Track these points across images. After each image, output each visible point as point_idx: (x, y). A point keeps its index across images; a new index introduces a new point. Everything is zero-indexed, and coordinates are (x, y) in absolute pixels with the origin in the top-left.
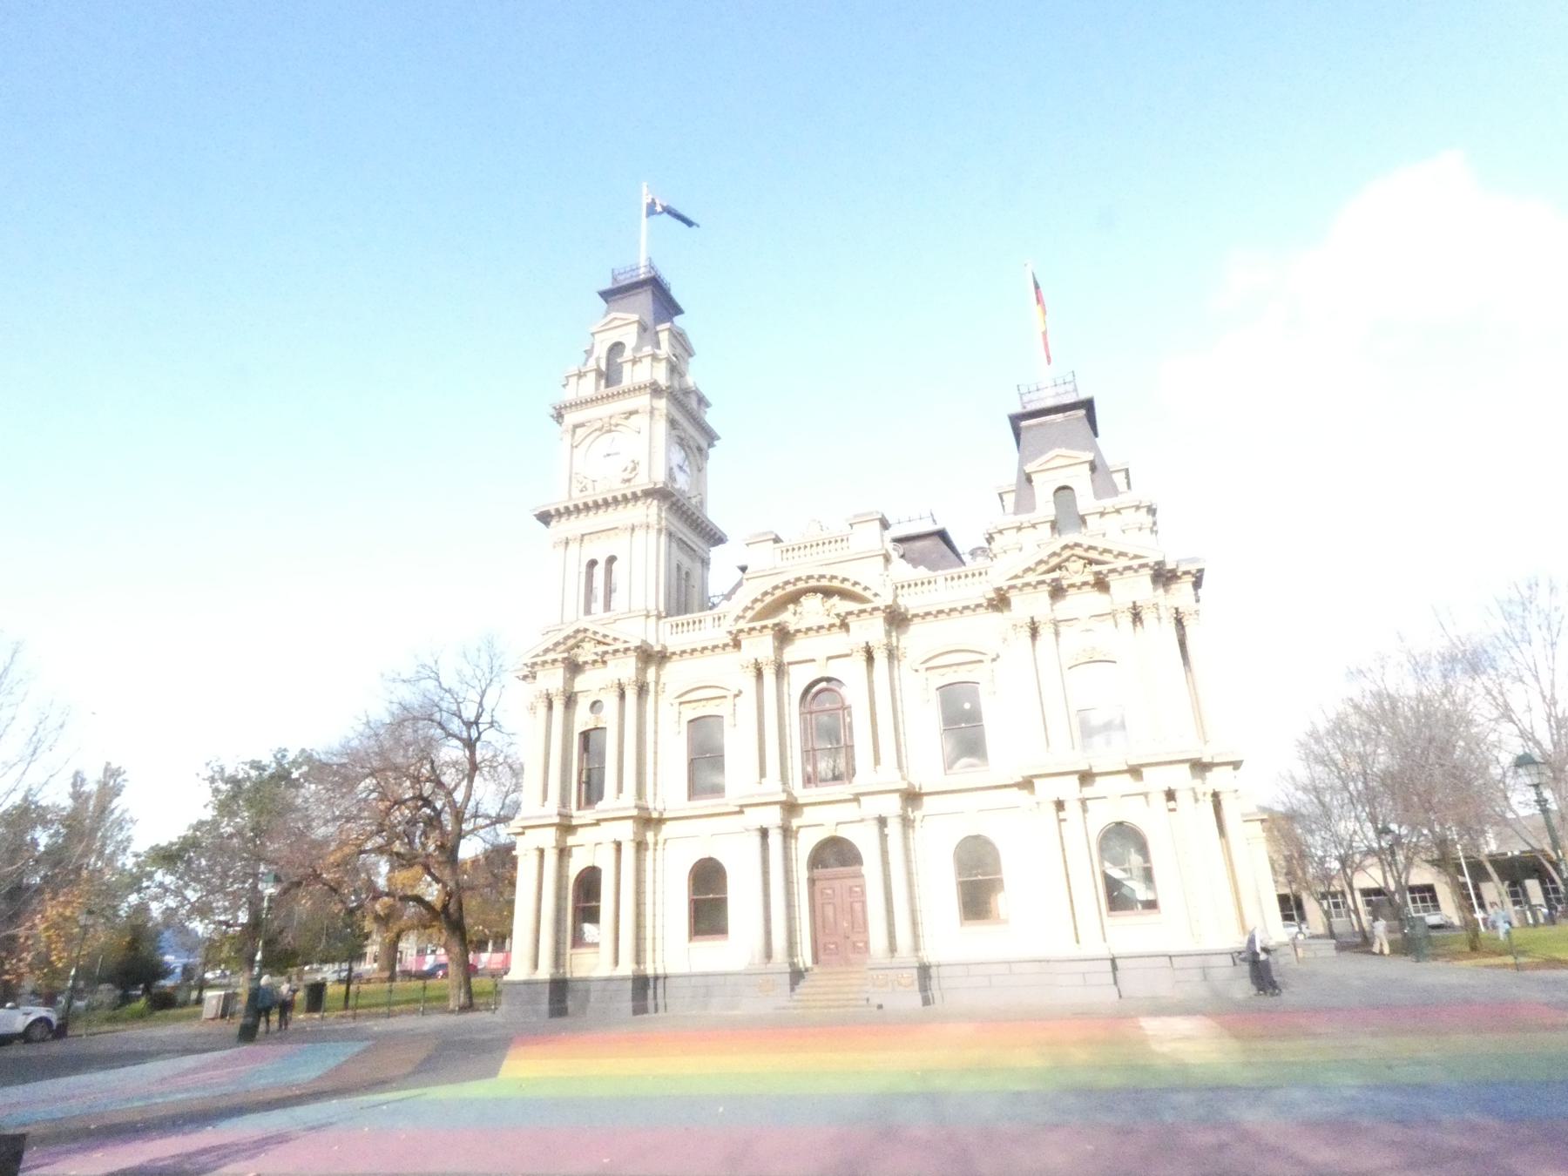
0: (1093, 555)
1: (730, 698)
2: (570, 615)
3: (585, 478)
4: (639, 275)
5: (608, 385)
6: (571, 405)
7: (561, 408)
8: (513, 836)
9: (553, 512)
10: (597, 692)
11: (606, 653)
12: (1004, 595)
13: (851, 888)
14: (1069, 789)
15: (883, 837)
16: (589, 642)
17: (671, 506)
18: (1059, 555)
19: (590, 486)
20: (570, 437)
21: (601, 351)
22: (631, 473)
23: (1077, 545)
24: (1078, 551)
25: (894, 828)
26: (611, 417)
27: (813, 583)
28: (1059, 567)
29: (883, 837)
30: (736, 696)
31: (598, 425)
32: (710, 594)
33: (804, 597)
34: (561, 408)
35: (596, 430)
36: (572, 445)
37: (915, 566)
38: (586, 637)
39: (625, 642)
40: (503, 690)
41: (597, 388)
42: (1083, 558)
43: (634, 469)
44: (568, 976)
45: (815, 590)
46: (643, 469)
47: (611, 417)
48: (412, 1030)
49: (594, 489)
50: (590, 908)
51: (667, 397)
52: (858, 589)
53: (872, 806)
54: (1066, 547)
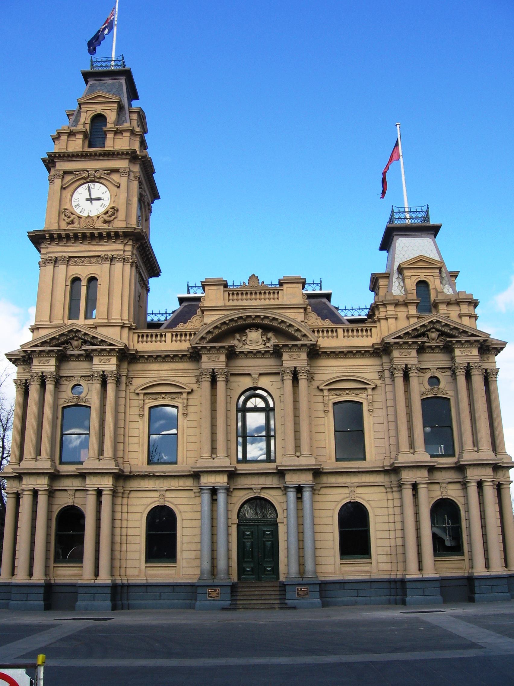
0: (446, 330)
3: (72, 214)
5: (90, 146)
6: (64, 156)
7: (55, 156)
11: (93, 350)
12: (279, 350)
13: (264, 532)
14: (306, 479)
15: (99, 503)
16: (77, 340)
17: (140, 246)
18: (67, 335)
19: (76, 221)
20: (60, 180)
21: (85, 118)
22: (110, 216)
23: (438, 322)
24: (438, 326)
25: (106, 499)
26: (96, 171)
27: (258, 321)
28: (423, 334)
29: (99, 503)
30: (189, 393)
31: (85, 175)
34: (55, 156)
35: (82, 178)
36: (62, 187)
37: (323, 319)
38: (76, 336)
39: (111, 344)
41: (83, 147)
42: (82, 339)
43: (113, 214)
44: (52, 582)
45: (257, 326)
46: (121, 214)
47: (96, 171)
49: (79, 223)
50: (342, 528)
51: (140, 164)
52: (291, 330)
53: (92, 483)
54: (431, 322)
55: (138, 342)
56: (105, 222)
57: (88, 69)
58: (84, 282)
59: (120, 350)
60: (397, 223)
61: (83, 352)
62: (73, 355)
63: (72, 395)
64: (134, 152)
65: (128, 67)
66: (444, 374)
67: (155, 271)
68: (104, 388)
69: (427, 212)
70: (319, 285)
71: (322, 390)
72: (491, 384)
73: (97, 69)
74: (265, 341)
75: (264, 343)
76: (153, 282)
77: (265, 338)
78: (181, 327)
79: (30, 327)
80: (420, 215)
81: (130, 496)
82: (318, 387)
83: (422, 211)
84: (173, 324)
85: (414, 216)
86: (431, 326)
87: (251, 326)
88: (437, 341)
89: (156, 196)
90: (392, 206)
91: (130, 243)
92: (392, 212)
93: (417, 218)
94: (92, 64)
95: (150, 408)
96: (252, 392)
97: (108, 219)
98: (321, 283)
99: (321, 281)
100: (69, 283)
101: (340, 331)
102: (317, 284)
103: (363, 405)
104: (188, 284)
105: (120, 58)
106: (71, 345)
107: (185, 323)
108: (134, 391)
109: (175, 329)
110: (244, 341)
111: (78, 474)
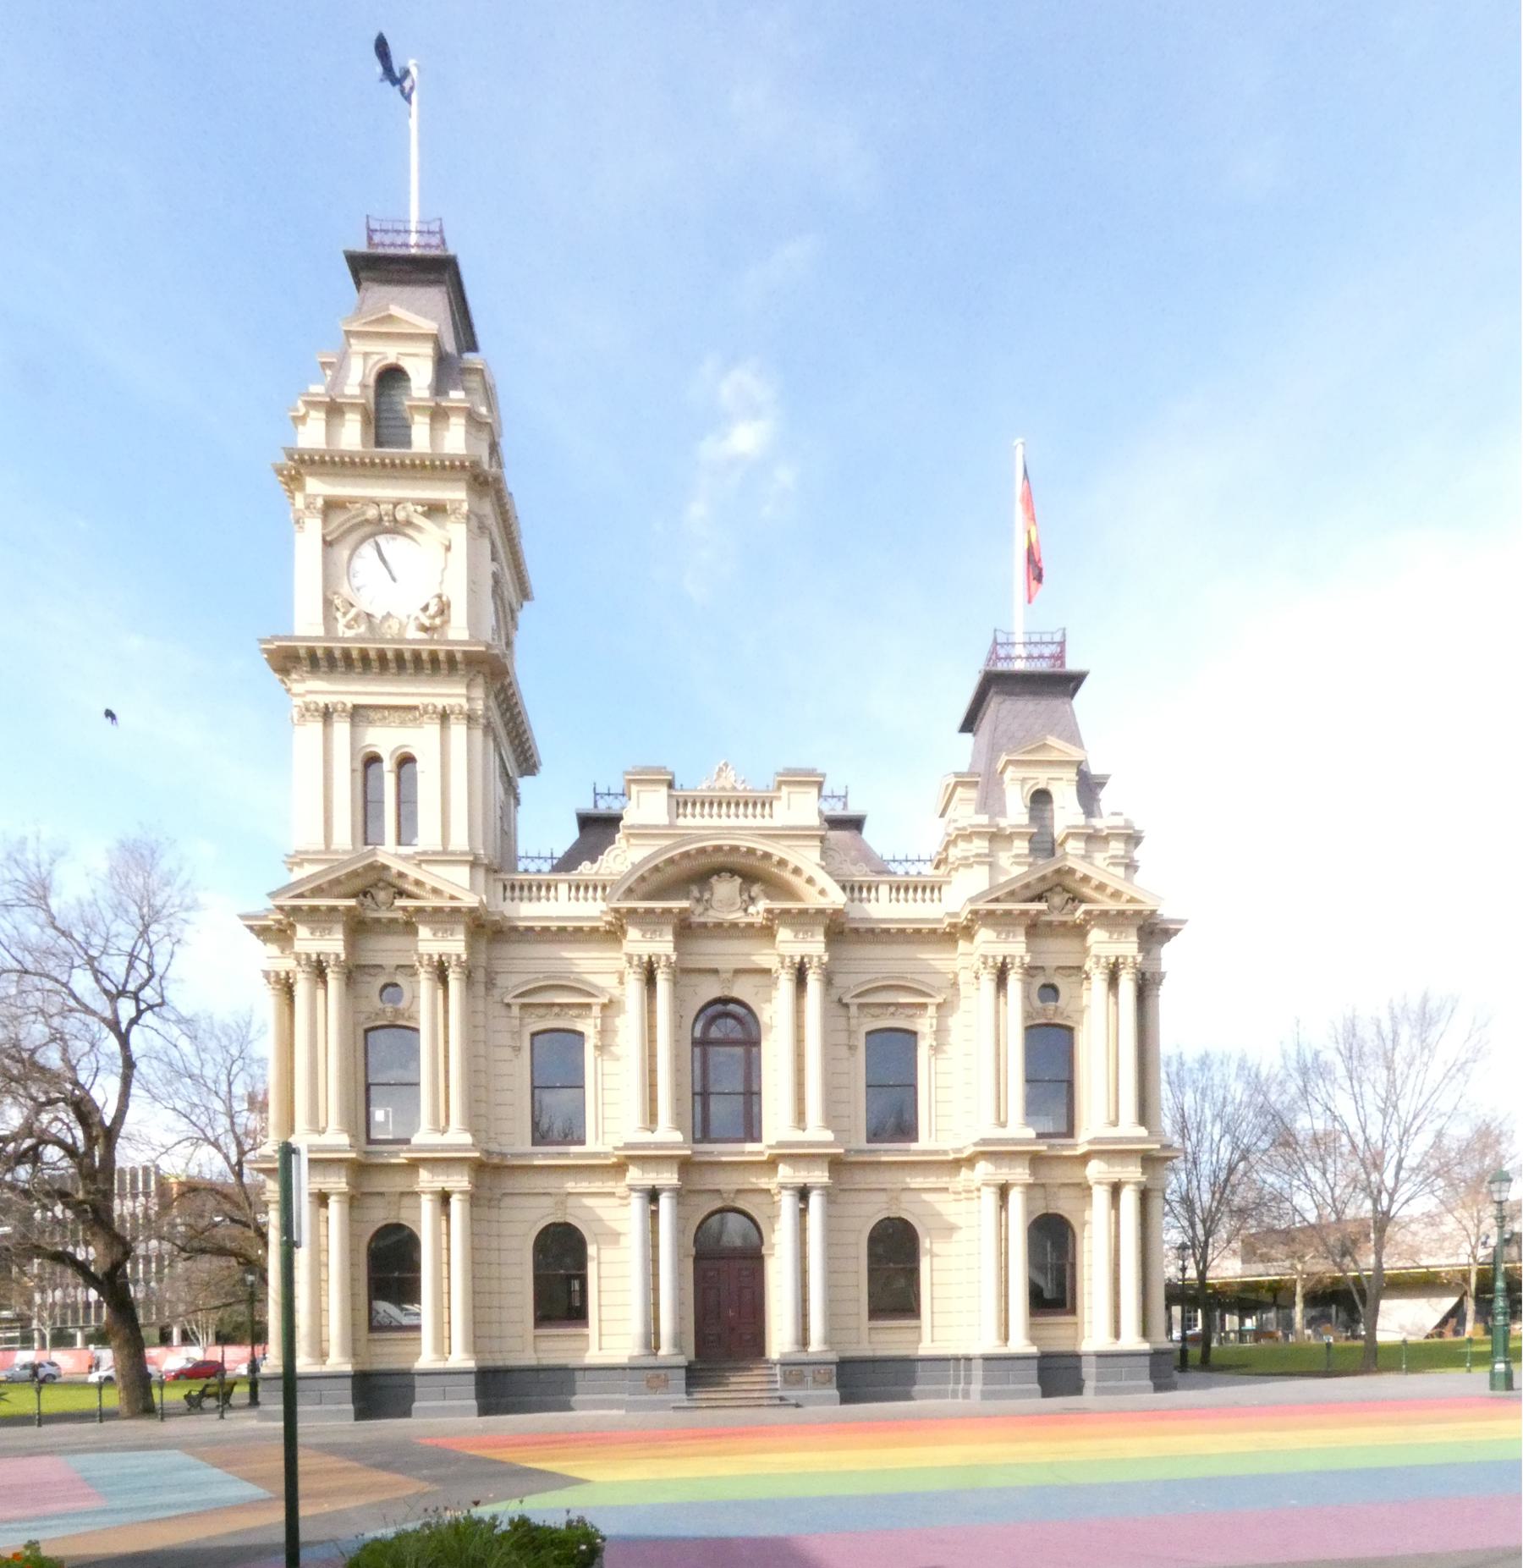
1: (596, 1011)
2: (343, 838)
4: (407, 246)
6: (323, 462)
8: (262, 1177)
9: (302, 653)
10: (392, 970)
31: (372, 513)
32: (521, 852)
33: (715, 877)
34: (302, 461)
36: (325, 542)
39: (452, 898)
40: (177, 948)
45: (733, 872)
48: (178, 1437)
55: (505, 899)
56: (425, 629)
57: (361, 247)
58: (388, 765)
59: (472, 910)
60: (1002, 667)
61: (400, 915)
62: (378, 920)
63: (380, 1005)
64: (475, 464)
65: (451, 251)
66: (1070, 980)
67: (527, 762)
68: (441, 352)
69: (1062, 644)
70: (843, 799)
71: (846, 1006)
72: (1150, 1002)
73: (380, 251)
74: (745, 901)
75: (744, 906)
76: (525, 784)
77: (745, 897)
78: (586, 869)
79: (285, 859)
80: (1047, 651)
81: (502, 1205)
82: (840, 1000)
83: (1053, 643)
84: (568, 863)
85: (1036, 653)
86: (1056, 879)
87: (718, 871)
88: (1064, 912)
89: (524, 593)
90: (995, 630)
91: (480, 680)
92: (996, 643)
93: (1041, 657)
94: (370, 238)
95: (534, 1035)
96: (719, 1008)
97: (427, 623)
98: (845, 797)
99: (847, 793)
100: (359, 766)
101: (884, 889)
102: (839, 798)
103: (864, 1081)
104: (595, 789)
105: (435, 227)
106: (373, 898)
107: (594, 860)
108: (499, 999)
109: (573, 876)
110: (707, 901)
111: (405, 1161)
